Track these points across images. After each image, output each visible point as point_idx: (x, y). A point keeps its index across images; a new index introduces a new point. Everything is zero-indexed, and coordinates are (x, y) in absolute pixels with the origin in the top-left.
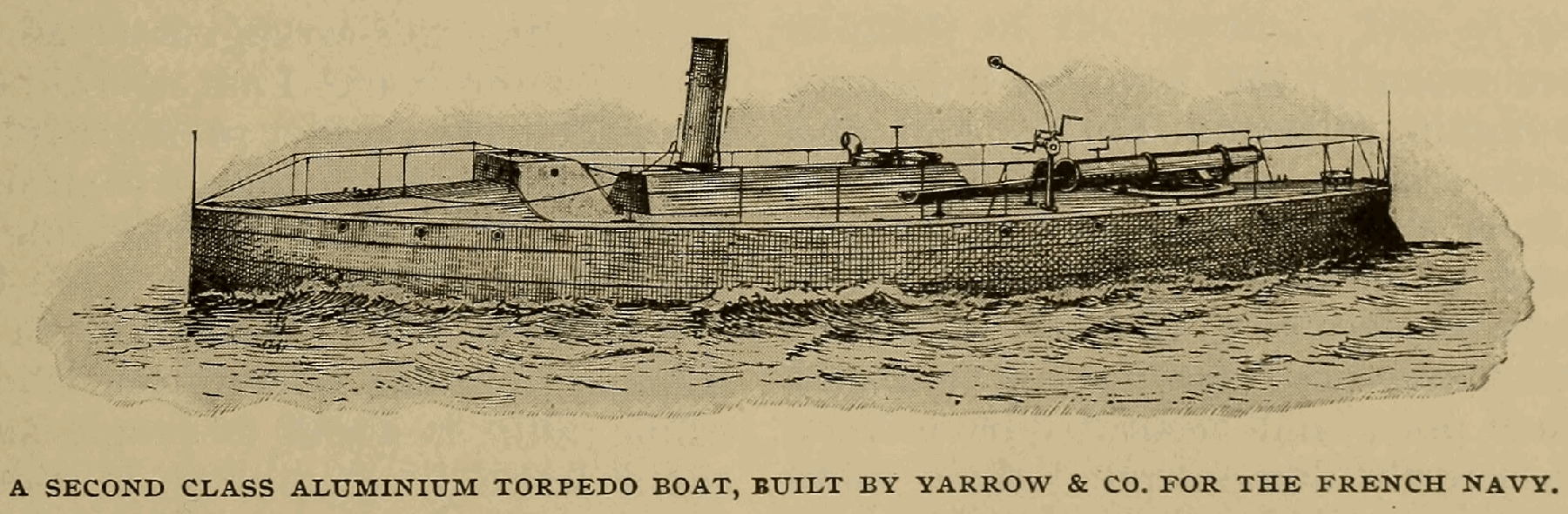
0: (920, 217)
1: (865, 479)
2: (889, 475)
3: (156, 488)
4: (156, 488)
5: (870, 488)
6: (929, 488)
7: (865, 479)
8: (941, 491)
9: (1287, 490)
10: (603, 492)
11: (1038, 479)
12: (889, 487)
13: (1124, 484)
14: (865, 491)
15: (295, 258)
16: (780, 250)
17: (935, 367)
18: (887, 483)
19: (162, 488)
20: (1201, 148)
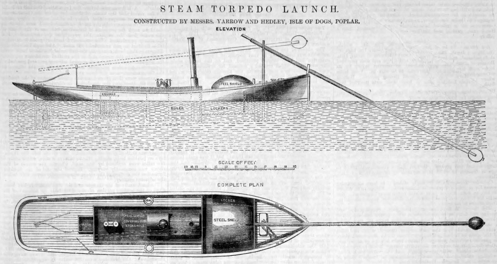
0: (78, 84)
1: (181, 20)
2: (186, 19)
3: (175, 21)
4: (175, 21)
5: (182, 22)
6: (186, 22)
7: (181, 20)
8: (222, 23)
9: (196, 23)
10: (174, 23)
11: (241, 20)
12: (186, 22)
13: (138, 21)
14: (181, 23)
15: (172, 119)
16: (12, 112)
17: (362, 126)
18: (283, 21)
19: (176, 21)
20: (196, 56)
